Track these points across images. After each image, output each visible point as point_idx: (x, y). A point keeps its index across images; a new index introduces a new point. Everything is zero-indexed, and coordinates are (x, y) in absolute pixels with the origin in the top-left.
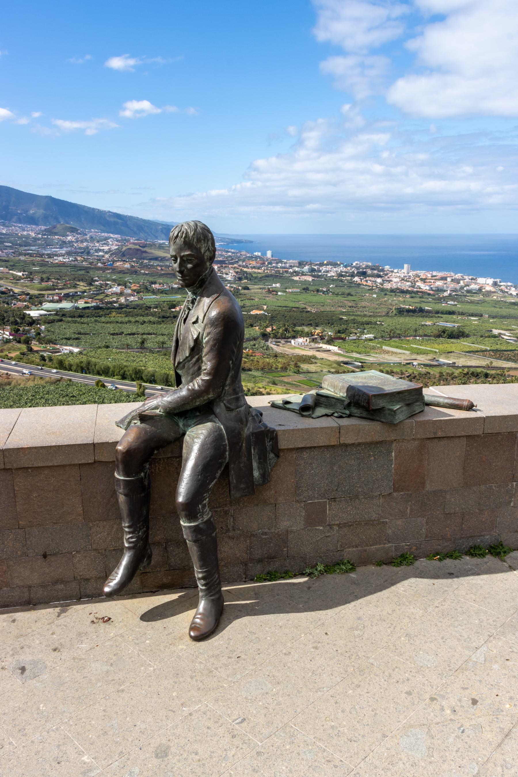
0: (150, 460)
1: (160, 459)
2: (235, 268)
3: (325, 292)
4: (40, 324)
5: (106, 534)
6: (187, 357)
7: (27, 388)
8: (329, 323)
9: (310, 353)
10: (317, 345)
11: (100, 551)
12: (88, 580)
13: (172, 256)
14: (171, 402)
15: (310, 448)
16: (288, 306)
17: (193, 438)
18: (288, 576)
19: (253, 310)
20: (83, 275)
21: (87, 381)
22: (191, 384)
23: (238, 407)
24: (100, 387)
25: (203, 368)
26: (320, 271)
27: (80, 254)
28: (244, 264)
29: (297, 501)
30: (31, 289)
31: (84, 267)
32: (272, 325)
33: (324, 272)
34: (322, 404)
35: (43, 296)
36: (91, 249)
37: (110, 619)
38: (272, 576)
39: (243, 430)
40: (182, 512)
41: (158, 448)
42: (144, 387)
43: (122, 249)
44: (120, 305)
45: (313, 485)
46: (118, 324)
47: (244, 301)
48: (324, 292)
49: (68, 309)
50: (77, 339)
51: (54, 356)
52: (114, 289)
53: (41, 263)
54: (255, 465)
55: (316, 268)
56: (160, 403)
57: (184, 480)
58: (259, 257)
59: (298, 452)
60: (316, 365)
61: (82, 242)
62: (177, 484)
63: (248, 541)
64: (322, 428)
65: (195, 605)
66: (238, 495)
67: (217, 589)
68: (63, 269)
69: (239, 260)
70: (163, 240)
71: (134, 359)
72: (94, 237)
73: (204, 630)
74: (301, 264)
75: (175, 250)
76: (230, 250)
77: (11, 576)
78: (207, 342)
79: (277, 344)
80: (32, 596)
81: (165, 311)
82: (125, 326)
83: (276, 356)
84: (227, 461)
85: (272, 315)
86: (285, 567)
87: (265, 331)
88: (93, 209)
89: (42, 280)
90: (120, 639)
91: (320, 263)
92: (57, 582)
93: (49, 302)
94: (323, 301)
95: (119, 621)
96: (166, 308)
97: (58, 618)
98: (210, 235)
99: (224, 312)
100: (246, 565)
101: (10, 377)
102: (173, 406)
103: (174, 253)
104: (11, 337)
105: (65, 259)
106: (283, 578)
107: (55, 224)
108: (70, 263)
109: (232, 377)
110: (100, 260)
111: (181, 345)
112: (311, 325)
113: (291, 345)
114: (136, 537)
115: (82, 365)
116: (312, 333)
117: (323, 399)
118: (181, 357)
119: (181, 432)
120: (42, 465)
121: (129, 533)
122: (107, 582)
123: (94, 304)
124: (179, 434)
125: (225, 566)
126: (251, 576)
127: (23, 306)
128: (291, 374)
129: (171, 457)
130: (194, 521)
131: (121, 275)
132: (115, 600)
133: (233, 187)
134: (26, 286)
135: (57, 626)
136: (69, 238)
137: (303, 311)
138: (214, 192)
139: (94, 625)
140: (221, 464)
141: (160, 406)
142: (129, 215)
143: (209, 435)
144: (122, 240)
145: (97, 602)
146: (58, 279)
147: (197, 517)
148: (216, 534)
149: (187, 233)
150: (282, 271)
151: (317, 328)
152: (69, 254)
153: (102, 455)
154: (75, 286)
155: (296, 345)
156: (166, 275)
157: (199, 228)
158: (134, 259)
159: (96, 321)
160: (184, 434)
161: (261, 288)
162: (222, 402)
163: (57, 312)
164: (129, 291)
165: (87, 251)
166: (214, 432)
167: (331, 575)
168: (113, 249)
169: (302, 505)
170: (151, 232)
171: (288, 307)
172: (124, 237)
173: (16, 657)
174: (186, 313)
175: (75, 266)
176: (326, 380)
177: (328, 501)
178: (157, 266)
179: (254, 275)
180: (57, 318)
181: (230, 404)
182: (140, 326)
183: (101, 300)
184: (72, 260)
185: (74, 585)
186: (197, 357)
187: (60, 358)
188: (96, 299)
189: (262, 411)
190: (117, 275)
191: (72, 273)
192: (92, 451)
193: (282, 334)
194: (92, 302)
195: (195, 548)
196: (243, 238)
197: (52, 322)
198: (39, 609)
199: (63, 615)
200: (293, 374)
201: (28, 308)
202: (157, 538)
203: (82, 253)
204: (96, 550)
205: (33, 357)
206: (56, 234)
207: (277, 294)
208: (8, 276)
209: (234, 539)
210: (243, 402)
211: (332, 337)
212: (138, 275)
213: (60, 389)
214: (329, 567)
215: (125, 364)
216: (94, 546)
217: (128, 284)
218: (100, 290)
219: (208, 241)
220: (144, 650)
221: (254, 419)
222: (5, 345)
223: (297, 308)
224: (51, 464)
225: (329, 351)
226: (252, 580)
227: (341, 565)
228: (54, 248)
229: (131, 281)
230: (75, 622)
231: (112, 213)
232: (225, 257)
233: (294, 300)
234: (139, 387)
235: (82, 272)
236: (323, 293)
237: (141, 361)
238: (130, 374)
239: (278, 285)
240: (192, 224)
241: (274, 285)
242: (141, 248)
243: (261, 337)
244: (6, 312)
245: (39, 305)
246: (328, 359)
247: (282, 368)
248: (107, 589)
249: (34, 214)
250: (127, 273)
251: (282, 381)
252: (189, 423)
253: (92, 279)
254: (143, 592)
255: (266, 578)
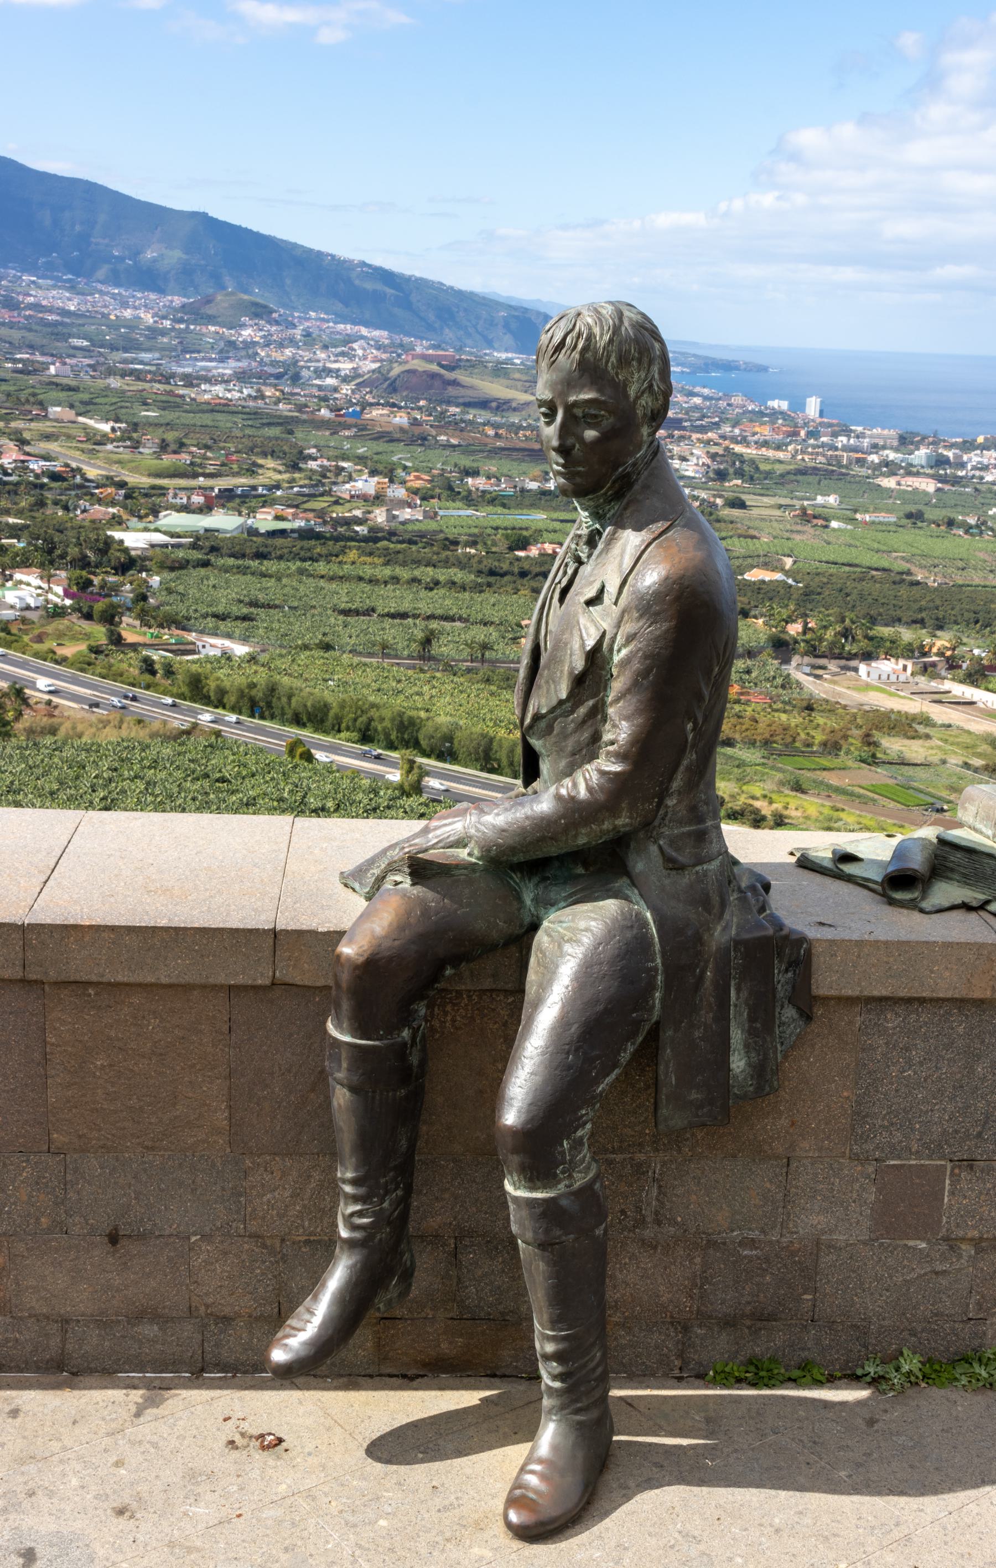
0: (432, 993)
1: (459, 993)
2: (708, 442)
3: (971, 527)
4: (147, 571)
5: (287, 1194)
6: (561, 703)
7: (99, 746)
8: (977, 622)
9: (913, 706)
10: (934, 685)
11: (269, 1242)
12: (226, 1320)
13: (542, 403)
14: (503, 831)
15: (909, 1001)
16: (857, 562)
17: (560, 942)
18: (808, 1378)
19: (753, 567)
20: (277, 439)
21: (263, 741)
22: (567, 782)
23: (700, 862)
24: (297, 760)
25: (607, 737)
26: (962, 465)
27: (272, 381)
28: (737, 431)
29: (855, 1157)
30: (132, 470)
31: (280, 417)
32: (807, 616)
33: (974, 468)
34: (952, 870)
35: (162, 491)
36: (303, 367)
37: (280, 1441)
38: (762, 1374)
39: (709, 929)
40: (510, 1157)
41: (456, 960)
42: (420, 767)
43: (389, 371)
44: (371, 530)
45: (906, 1112)
46: (362, 585)
47: (729, 541)
48: (968, 529)
49: (226, 531)
50: (245, 618)
51: (180, 663)
52: (359, 484)
53: (164, 398)
54: (737, 1036)
55: (950, 454)
56: (473, 831)
57: (526, 1061)
58: (782, 413)
59: (869, 1011)
60: (928, 743)
61: (281, 345)
62: (503, 1071)
63: (698, 1260)
64: (948, 945)
65: (529, 1432)
66: (678, 1121)
67: (597, 1394)
68: (224, 421)
69: (721, 420)
70: (506, 351)
71: (400, 686)
72: (315, 333)
73: (550, 1510)
74: (906, 441)
75: (552, 386)
76: (697, 389)
77: (18, 1284)
78: (625, 663)
79: (816, 672)
80: (69, 1347)
81: (499, 557)
82: (381, 590)
83: (810, 708)
84: (655, 1018)
85: (806, 587)
86: (803, 1349)
87: (784, 631)
88: (319, 253)
89: (164, 447)
90: (304, 1505)
91: (965, 442)
92: (140, 1316)
93: (178, 511)
94: (965, 556)
95: (307, 1450)
96: (502, 547)
97: (136, 1421)
98: (657, 345)
99: (682, 577)
100: (686, 1329)
101: (56, 713)
102: (510, 842)
103: (547, 395)
104: (68, 602)
105: (229, 391)
106: (793, 1382)
107: (211, 291)
108: (243, 403)
109: (688, 769)
110: (325, 399)
111: (547, 666)
112: (922, 623)
113: (858, 679)
114: (374, 1214)
115: (254, 692)
116: (922, 646)
117: (957, 857)
118: (543, 701)
119: (527, 920)
120: (125, 979)
121: (355, 1199)
122: (279, 1335)
123: (299, 524)
124: (521, 926)
125: (623, 1325)
126: (701, 1364)
127: (107, 517)
128: (850, 763)
129: (492, 990)
130: (545, 1187)
131: (381, 446)
132: (299, 1388)
133: (723, 207)
134: (119, 462)
135: (132, 1443)
136: (247, 333)
137: (902, 579)
138: (664, 220)
139: (235, 1454)
140: (638, 1024)
141: (471, 837)
142: (418, 274)
143: (609, 935)
144: (393, 345)
145: (246, 1389)
146: (207, 447)
147: (555, 1175)
148: (606, 1231)
149: (590, 337)
150: (849, 458)
151: (939, 633)
152: (242, 377)
153: (295, 966)
154: (252, 470)
155: (873, 680)
156: (508, 452)
157: (626, 323)
158: (422, 403)
159: (301, 572)
160: (534, 927)
161: (780, 506)
162: (655, 842)
163: (198, 538)
164: (399, 492)
165: (292, 373)
166: (624, 928)
167: (943, 1392)
168: (365, 369)
169: (871, 1169)
170: (475, 327)
171: (856, 566)
172: (397, 338)
173: (12, 1517)
174: (570, 571)
175: (255, 414)
176: (971, 800)
177: (949, 1165)
178: (484, 424)
179: (763, 467)
180: (197, 555)
181: (677, 850)
182: (423, 593)
183: (321, 514)
184: (250, 396)
185: (188, 1330)
186: (591, 703)
187: (194, 668)
188: (306, 510)
189: (769, 878)
190: (369, 443)
191: (248, 431)
192: (268, 953)
193: (833, 644)
194: (295, 516)
195: (542, 1266)
196: (741, 358)
197: (181, 566)
198: (85, 1388)
199: (151, 1412)
200: (857, 765)
201: (120, 523)
202: (433, 1223)
203: (279, 376)
204: (255, 1236)
205: (121, 661)
206: (211, 320)
207: (826, 527)
208: (73, 432)
209: (655, 1248)
210: (715, 848)
211: (985, 662)
212: (429, 447)
213: (187, 755)
214: (937, 1367)
215: (372, 698)
216: (253, 1226)
217: (400, 473)
218: (320, 483)
219: (650, 363)
220: (372, 1546)
221: (743, 900)
222: (49, 624)
223: (884, 570)
224: (150, 979)
225: (972, 703)
226: (701, 1377)
227: (976, 1365)
228: (203, 359)
229: (409, 464)
230: (181, 1438)
231: (369, 266)
232: (682, 409)
233: (876, 546)
234: (406, 766)
235: (275, 431)
236: (967, 532)
237: (418, 694)
238: (384, 729)
239: (832, 500)
240: (607, 311)
241: (820, 499)
242: (442, 371)
243: (769, 650)
244: (61, 532)
245: (151, 518)
246: (967, 727)
247: (824, 744)
248: (279, 1356)
249: (154, 260)
250: (398, 440)
251: (822, 783)
252: (553, 895)
253: (301, 452)
254: (380, 1375)
255: (743, 1375)
